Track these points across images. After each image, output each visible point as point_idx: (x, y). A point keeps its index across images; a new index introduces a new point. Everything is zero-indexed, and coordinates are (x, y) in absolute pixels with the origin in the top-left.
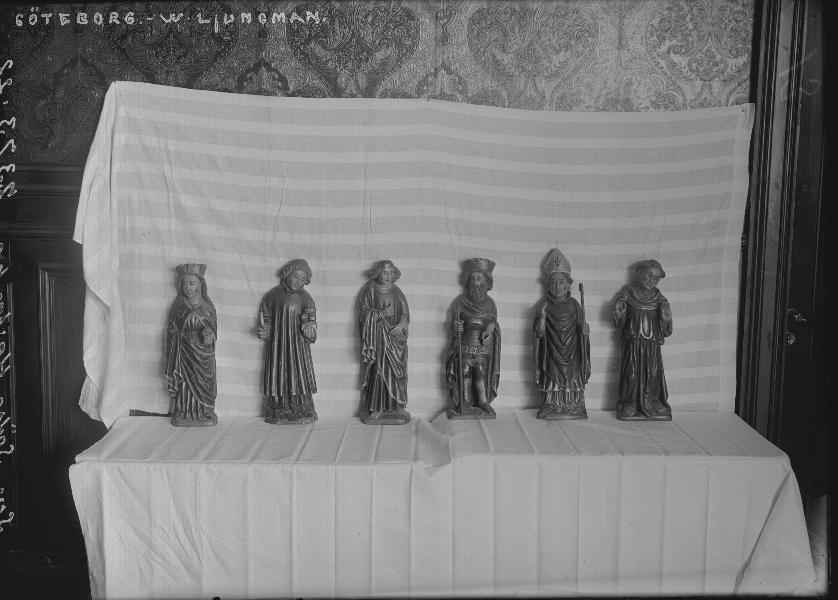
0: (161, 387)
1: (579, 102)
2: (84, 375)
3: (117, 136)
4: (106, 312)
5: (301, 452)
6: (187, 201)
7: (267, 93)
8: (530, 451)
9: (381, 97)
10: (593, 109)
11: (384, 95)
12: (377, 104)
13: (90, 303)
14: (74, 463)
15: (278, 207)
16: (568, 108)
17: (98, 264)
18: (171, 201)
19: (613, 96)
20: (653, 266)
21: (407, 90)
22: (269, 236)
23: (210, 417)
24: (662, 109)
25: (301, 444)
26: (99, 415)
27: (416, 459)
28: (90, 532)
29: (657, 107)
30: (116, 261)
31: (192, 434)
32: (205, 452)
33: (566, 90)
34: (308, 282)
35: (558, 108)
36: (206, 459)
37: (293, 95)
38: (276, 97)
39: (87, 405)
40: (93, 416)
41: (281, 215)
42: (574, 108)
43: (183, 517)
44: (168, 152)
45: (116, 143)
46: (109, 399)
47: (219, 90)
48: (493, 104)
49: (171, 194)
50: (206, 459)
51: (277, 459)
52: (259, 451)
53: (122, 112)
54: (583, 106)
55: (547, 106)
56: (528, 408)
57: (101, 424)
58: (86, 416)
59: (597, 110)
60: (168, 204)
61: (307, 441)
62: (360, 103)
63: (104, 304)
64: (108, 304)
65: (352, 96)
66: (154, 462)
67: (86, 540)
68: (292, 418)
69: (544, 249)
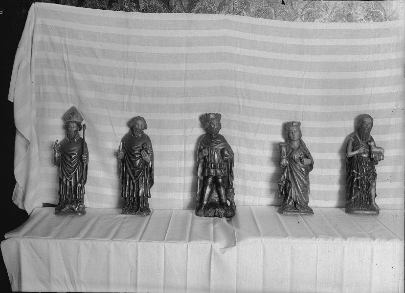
0: (269, 188)
1: (319, 16)
2: (15, 182)
3: (35, 36)
4: (28, 145)
5: (143, 233)
6: (77, 76)
7: (126, 10)
8: (286, 236)
9: (196, 12)
10: (327, 21)
11: (198, 12)
12: (193, 17)
13: (18, 138)
14: (4, 239)
15: (133, 80)
16: (312, 20)
17: (23, 116)
18: (68, 76)
19: (341, 12)
20: (367, 117)
21: (212, 8)
22: (126, 98)
23: (83, 212)
24: (371, 20)
25: (143, 227)
26: (23, 205)
27: (215, 241)
28: (14, 281)
29: (369, 19)
30: (34, 113)
31: (360, 220)
32: (83, 233)
33: (201, 6)
34: (146, 128)
35: (306, 20)
36: (85, 237)
37: (142, 11)
38: (132, 12)
39: (18, 201)
40: (20, 207)
41: (134, 85)
42: (315, 20)
43: (69, 270)
44: (65, 45)
45: (35, 40)
46: (30, 196)
47: (97, 8)
48: (265, 17)
49: (67, 72)
50: (85, 237)
51: (130, 237)
52: (117, 232)
53: (39, 21)
54: (322, 19)
55: (299, 19)
56: (337, 207)
57: (25, 212)
58: (17, 207)
59: (331, 21)
60: (66, 77)
61: (147, 225)
62: (183, 17)
63: (26, 139)
64: (29, 140)
65: (179, 12)
66: (52, 239)
67: (12, 286)
68: (72, 212)
69: (68, 107)
